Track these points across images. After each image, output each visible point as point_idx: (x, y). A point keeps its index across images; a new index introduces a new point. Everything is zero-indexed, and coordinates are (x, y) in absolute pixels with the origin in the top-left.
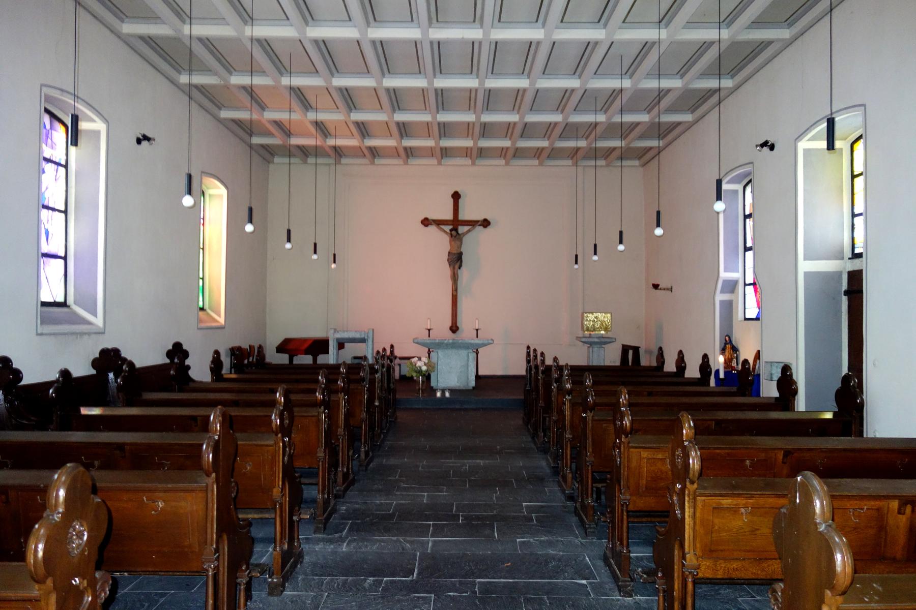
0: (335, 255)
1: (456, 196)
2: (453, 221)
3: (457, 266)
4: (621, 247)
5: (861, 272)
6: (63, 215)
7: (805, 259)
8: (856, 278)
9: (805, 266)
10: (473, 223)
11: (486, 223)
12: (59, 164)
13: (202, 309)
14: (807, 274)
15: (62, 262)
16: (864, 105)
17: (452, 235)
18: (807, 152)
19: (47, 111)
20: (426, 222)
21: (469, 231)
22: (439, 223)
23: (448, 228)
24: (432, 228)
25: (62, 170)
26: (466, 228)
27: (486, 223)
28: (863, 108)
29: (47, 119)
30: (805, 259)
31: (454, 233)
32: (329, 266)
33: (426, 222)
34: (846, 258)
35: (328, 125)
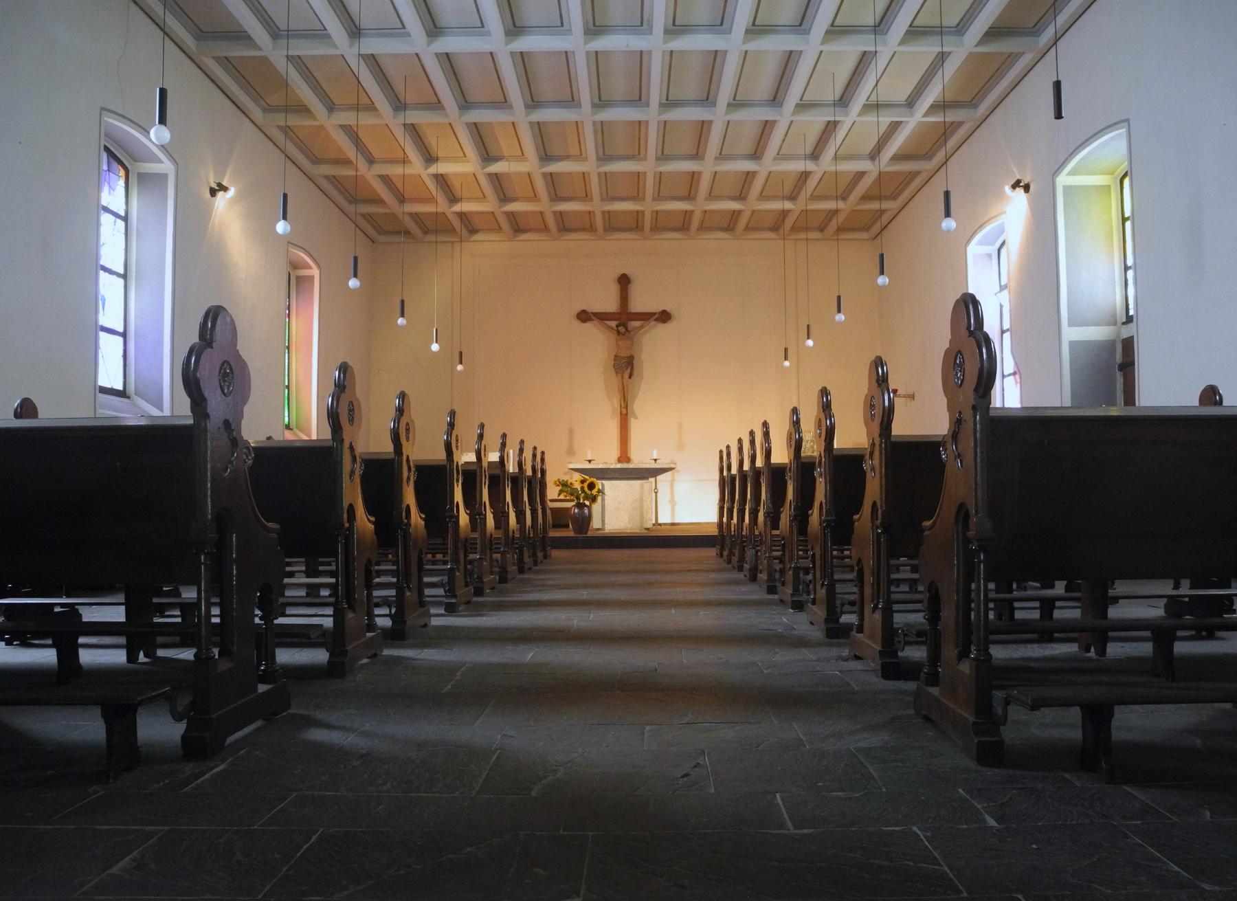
0: (461, 353)
1: (624, 281)
2: (583, 522)
3: (626, 376)
4: (841, 317)
5: (1132, 337)
6: (121, 281)
7: (1070, 325)
8: (1128, 345)
9: (1071, 334)
10: (646, 317)
11: (664, 317)
12: (117, 215)
13: (288, 427)
14: (1073, 344)
15: (121, 339)
16: (1127, 120)
17: (619, 333)
18: (1068, 190)
19: (107, 149)
20: (584, 316)
21: (642, 327)
22: (602, 317)
23: (613, 324)
24: (591, 328)
25: (121, 224)
26: (637, 324)
27: (664, 317)
28: (1126, 124)
29: (105, 156)
30: (1070, 325)
31: (622, 329)
32: (453, 369)
33: (584, 316)
34: (1119, 323)
35: (456, 184)
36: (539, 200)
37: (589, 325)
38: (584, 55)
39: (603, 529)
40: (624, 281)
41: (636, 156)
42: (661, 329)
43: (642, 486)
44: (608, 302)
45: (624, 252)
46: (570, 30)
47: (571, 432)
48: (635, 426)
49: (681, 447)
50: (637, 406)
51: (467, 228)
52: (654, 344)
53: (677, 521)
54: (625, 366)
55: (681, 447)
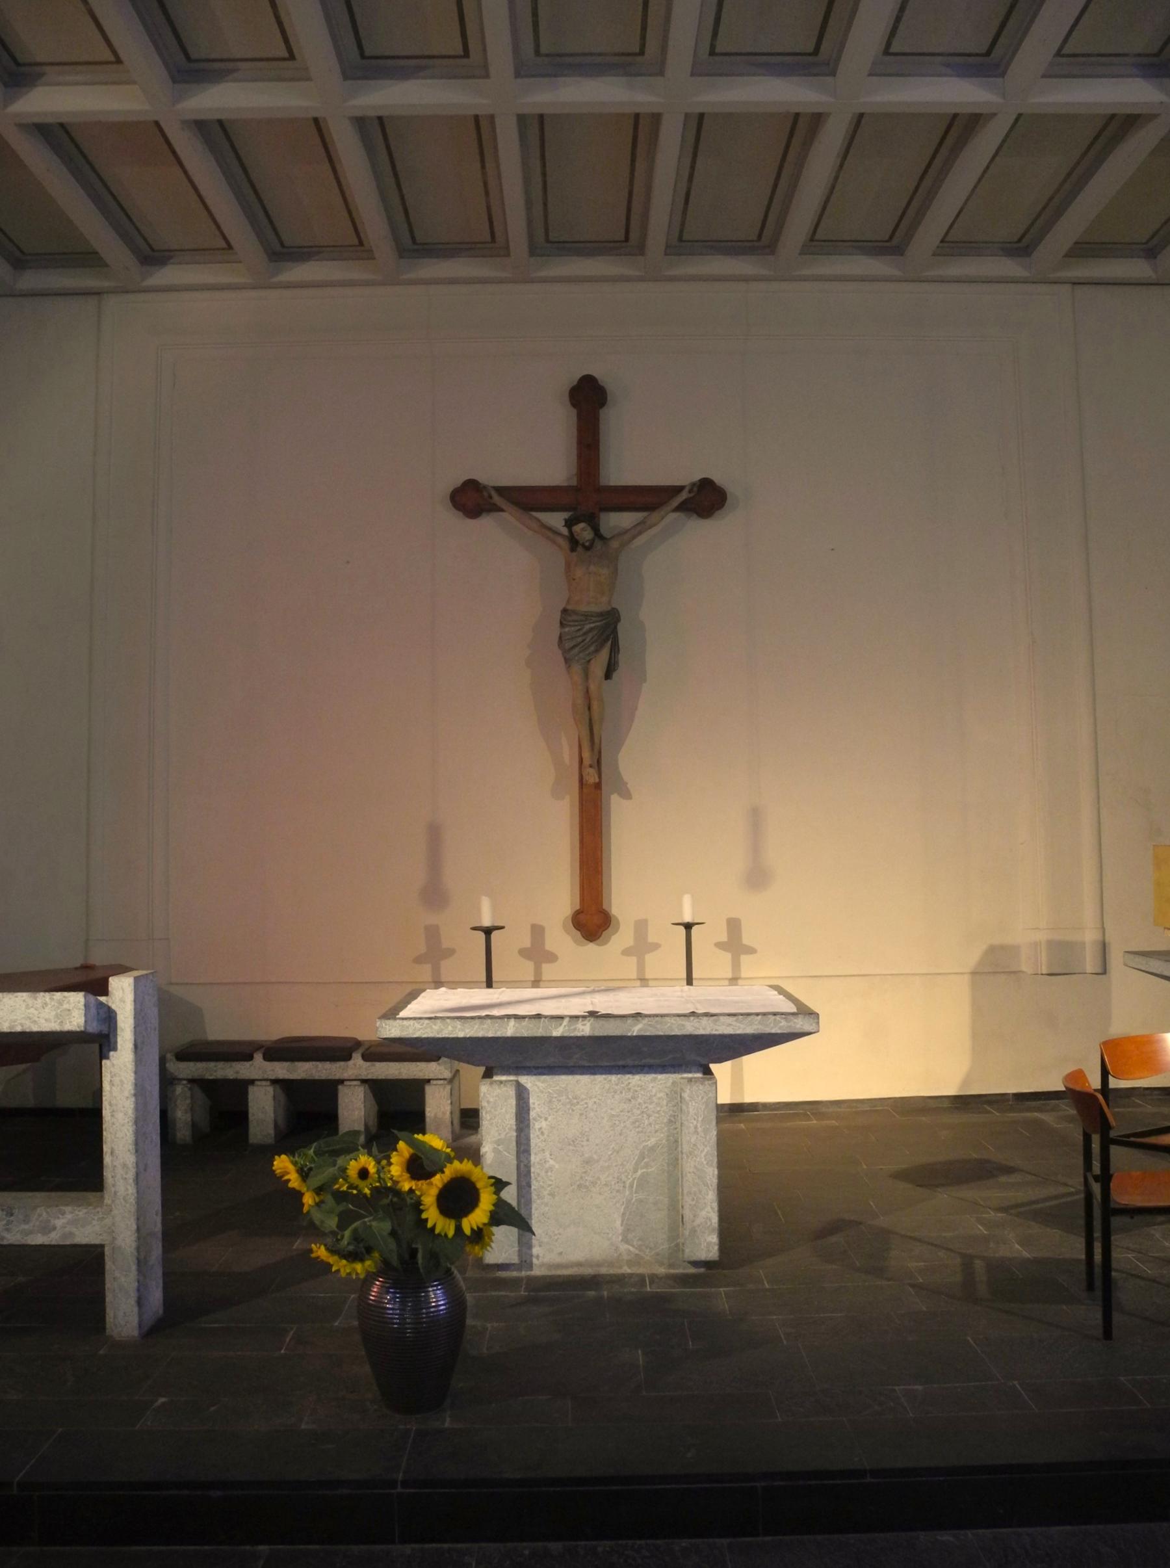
1: (588, 397)
10: (649, 499)
11: (706, 499)
20: (471, 499)
21: (640, 528)
22: (527, 500)
23: (556, 520)
27: (706, 499)
31: (583, 531)
33: (471, 499)
36: (304, 76)
37: (486, 523)
38: (513, 123)
39: (525, 1262)
40: (588, 397)
41: (629, 62)
42: (695, 537)
43: (676, 1098)
44: (549, 462)
45: (590, 314)
46: (507, 248)
47: (435, 835)
48: (625, 823)
49: (757, 877)
50: (630, 760)
51: (136, 251)
52: (676, 578)
53: (748, 1099)
54: (595, 642)
55: (757, 877)
